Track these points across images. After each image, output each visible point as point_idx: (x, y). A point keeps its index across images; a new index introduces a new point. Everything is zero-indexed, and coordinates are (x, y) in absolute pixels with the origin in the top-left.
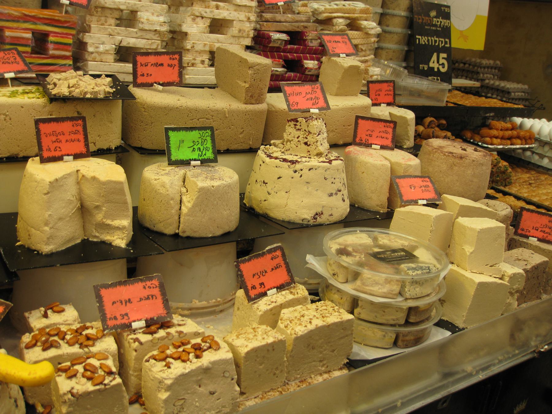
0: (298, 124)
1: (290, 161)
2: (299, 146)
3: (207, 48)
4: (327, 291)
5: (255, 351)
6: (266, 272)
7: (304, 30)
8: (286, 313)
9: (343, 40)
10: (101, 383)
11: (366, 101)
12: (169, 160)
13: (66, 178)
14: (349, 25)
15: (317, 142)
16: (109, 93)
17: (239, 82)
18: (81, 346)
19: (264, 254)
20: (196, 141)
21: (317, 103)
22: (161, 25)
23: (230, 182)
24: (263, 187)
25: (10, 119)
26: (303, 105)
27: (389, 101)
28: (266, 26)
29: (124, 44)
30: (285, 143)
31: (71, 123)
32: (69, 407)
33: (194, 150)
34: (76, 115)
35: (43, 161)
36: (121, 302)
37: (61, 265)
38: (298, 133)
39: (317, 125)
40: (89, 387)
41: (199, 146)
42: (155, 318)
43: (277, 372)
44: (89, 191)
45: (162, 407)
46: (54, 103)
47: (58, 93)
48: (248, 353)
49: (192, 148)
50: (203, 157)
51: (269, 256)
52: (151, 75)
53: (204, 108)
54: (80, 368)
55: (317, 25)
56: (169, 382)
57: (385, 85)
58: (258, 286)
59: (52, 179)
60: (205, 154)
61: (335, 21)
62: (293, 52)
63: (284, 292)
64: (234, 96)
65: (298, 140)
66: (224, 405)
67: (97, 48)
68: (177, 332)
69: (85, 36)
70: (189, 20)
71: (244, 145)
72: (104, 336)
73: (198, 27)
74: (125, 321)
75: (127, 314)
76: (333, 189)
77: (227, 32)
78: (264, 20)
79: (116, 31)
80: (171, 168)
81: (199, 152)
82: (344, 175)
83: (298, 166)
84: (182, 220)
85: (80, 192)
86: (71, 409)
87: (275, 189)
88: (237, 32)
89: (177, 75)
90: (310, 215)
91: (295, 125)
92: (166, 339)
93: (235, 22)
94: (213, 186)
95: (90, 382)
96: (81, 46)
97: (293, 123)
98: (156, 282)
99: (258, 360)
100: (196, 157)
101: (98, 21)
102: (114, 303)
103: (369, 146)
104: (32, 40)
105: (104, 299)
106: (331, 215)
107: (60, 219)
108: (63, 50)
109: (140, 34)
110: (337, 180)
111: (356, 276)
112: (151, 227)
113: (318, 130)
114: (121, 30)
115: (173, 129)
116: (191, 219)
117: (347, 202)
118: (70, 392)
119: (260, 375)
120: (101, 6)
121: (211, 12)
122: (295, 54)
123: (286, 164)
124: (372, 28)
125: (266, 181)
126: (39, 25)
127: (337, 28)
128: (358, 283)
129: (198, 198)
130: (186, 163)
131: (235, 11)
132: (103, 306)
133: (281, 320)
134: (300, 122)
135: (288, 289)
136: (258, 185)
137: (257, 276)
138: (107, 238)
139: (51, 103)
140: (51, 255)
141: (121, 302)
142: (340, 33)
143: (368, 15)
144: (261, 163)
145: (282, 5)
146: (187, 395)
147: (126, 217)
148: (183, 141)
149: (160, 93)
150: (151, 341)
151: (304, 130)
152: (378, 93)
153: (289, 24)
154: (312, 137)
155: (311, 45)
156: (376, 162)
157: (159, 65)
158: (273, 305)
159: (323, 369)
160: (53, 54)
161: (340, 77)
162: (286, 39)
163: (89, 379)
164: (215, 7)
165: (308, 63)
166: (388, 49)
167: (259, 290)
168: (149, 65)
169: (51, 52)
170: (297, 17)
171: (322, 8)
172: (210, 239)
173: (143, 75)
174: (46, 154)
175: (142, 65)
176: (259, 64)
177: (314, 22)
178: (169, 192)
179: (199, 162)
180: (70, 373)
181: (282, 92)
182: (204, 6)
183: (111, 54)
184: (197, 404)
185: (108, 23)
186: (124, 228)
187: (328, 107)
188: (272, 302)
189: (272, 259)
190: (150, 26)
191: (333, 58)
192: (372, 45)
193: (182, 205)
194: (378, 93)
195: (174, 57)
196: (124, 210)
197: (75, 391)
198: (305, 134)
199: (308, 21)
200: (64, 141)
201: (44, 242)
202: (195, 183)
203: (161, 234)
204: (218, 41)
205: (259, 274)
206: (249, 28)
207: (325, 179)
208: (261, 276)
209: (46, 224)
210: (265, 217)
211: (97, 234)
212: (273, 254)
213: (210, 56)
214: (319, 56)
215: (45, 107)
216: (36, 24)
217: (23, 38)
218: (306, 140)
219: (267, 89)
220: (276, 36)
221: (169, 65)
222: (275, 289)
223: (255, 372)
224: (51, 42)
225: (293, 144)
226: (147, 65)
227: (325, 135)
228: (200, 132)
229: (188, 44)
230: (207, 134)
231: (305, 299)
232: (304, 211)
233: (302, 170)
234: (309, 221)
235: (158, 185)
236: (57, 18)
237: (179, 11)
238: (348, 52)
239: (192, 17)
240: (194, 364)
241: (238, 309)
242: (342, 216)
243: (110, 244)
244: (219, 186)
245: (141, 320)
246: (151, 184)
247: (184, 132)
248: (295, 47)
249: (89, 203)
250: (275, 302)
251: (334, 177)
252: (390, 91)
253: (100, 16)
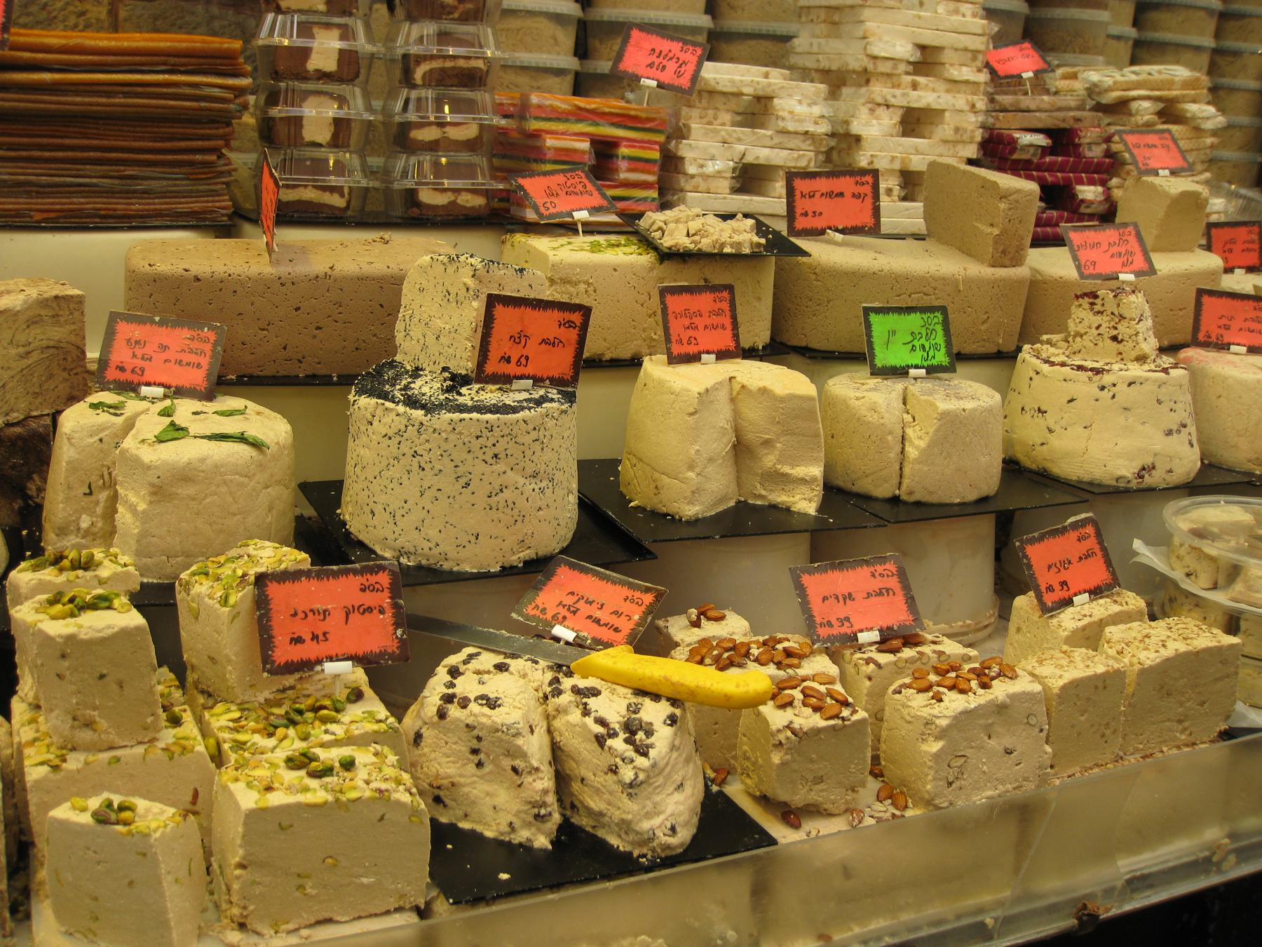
0: (1097, 301)
1: (1091, 370)
2: (1100, 344)
3: (897, 166)
4: (1171, 608)
5: (1075, 685)
6: (1070, 563)
7: (1076, 126)
8: (1113, 632)
9: (1163, 142)
10: (837, 716)
11: (1214, 261)
12: (873, 366)
13: (717, 389)
14: (1160, 114)
15: (1137, 334)
16: (759, 245)
17: (979, 225)
18: (779, 665)
19: (1064, 531)
20: (916, 332)
21: (1132, 263)
22: (816, 123)
23: (991, 403)
24: (1037, 420)
25: (595, 291)
26: (1105, 267)
27: (1250, 263)
28: (1005, 122)
29: (749, 159)
30: (1070, 339)
31: (713, 295)
32: (786, 754)
33: (913, 349)
34: (702, 283)
35: (674, 360)
36: (837, 598)
37: (721, 537)
38: (1097, 319)
39: (1136, 302)
40: (817, 721)
41: (923, 341)
42: (895, 628)
43: (1108, 732)
44: (753, 414)
45: (930, 768)
46: (666, 262)
47: (677, 244)
48: (1064, 688)
49: (910, 345)
50: (929, 363)
51: (1073, 535)
52: (821, 214)
53: (922, 273)
54: (797, 694)
55: (1100, 114)
56: (944, 722)
57: (1242, 231)
58: (1057, 587)
59: (702, 389)
60: (934, 357)
61: (1134, 105)
62: (1056, 169)
63: (1102, 601)
64: (967, 250)
65: (1099, 331)
66: (1026, 775)
67: (702, 166)
68: (934, 652)
69: (680, 146)
70: (864, 113)
71: (987, 344)
72: (812, 653)
73: (880, 124)
74: (846, 629)
75: (847, 619)
76: (1173, 421)
77: (931, 132)
78: (997, 108)
79: (735, 135)
80: (876, 380)
81: (922, 352)
82: (1189, 398)
83: (1107, 379)
84: (907, 470)
85: (737, 414)
86: (788, 757)
87: (1063, 423)
88: (952, 132)
89: (870, 212)
90: (1132, 470)
91: (1092, 304)
92: (918, 663)
93: (947, 114)
94: (964, 410)
95: (818, 714)
96: (670, 164)
97: (1087, 299)
98: (891, 567)
99: (1079, 703)
100: (918, 362)
101: (701, 117)
102: (825, 599)
103: (1223, 349)
104: (591, 153)
105: (809, 591)
106: (1170, 471)
107: (711, 460)
108: (643, 171)
109: (776, 140)
110: (1179, 405)
111: (1234, 572)
112: (848, 486)
113: (1139, 312)
114: (743, 133)
115: (878, 311)
116: (926, 468)
117: (1197, 449)
118: (788, 727)
119: (1080, 734)
120: (709, 88)
121: (904, 95)
122: (1059, 174)
123: (1083, 375)
124: (1208, 118)
125: (1043, 408)
126: (603, 126)
127: (1141, 120)
128: (1239, 587)
129: (937, 430)
130: (900, 372)
131: (948, 91)
132: (808, 603)
133: (1108, 642)
134: (1101, 297)
135: (1107, 597)
136: (1027, 416)
137: (1054, 570)
138: (781, 498)
139: (661, 263)
140: (695, 522)
141: (837, 598)
142: (1144, 129)
143: (1198, 91)
144: (1033, 374)
145: (1029, 79)
146: (970, 750)
147: (815, 461)
148: (894, 332)
149: (838, 248)
150: (895, 663)
151: (1109, 313)
152: (1228, 246)
153: (1046, 114)
154: (1127, 325)
155: (1089, 154)
156: (1245, 376)
157: (836, 195)
158: (1086, 621)
159: (1183, 737)
160: (625, 179)
161: (1161, 214)
162: (1044, 144)
163: (816, 709)
164: (910, 85)
165: (1084, 191)
166: (1221, 161)
167: (1059, 594)
168: (818, 195)
169: (623, 176)
170: (1061, 101)
171: (1108, 81)
172: (957, 508)
173: (806, 214)
174: (676, 349)
175: (803, 196)
176: (1018, 191)
177: (1090, 110)
178: (886, 421)
179: (924, 371)
180: (780, 701)
181: (1065, 245)
182: (890, 85)
183: (726, 178)
184: (985, 768)
185: (719, 121)
186: (814, 479)
187: (1152, 271)
188: (1085, 616)
189: (1079, 540)
190: (797, 124)
191: (1145, 178)
192: (1208, 151)
193: (907, 444)
194: (1228, 246)
195: (864, 179)
196: (813, 449)
197: (796, 726)
198: (1113, 320)
199: (1080, 108)
200: (701, 327)
201: (685, 498)
202: (932, 405)
203: (868, 498)
204: (916, 150)
205: (1058, 565)
206: (973, 125)
207: (1159, 402)
208: (1062, 569)
209: (691, 467)
210: (1043, 475)
211: (764, 492)
212: (1081, 530)
213: (901, 179)
214: (1105, 176)
215: (652, 269)
216: (598, 125)
217: (575, 151)
218: (1115, 332)
219: (1028, 241)
220: (1026, 139)
221: (854, 195)
222: (1087, 594)
223: (1073, 726)
224: (624, 158)
225: (1087, 341)
226: (813, 196)
227: (1149, 323)
228: (923, 316)
229: (862, 158)
230: (936, 320)
231: (1140, 613)
232: (1120, 462)
233: (1114, 385)
234: (1129, 482)
235: (864, 408)
236: (633, 113)
237: (841, 94)
238: (1174, 165)
239: (870, 106)
240: (977, 698)
241: (1018, 630)
242: (1188, 474)
243: (788, 510)
244: (975, 410)
245: (871, 629)
246: (848, 407)
247: (896, 316)
248: (1060, 159)
249: (751, 436)
250: (1090, 616)
251: (1175, 399)
252: (1253, 242)
253: (705, 109)
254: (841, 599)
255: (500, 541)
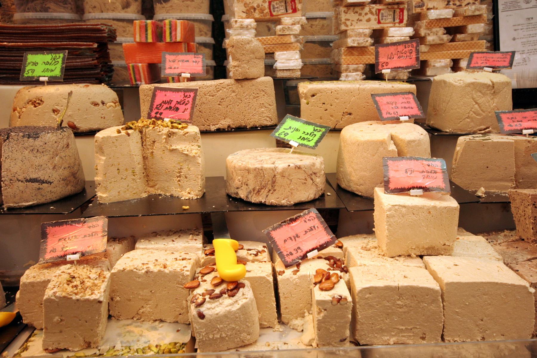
75: (299, 248)
102: (285, 241)
254: (293, 238)
255: (244, 187)
